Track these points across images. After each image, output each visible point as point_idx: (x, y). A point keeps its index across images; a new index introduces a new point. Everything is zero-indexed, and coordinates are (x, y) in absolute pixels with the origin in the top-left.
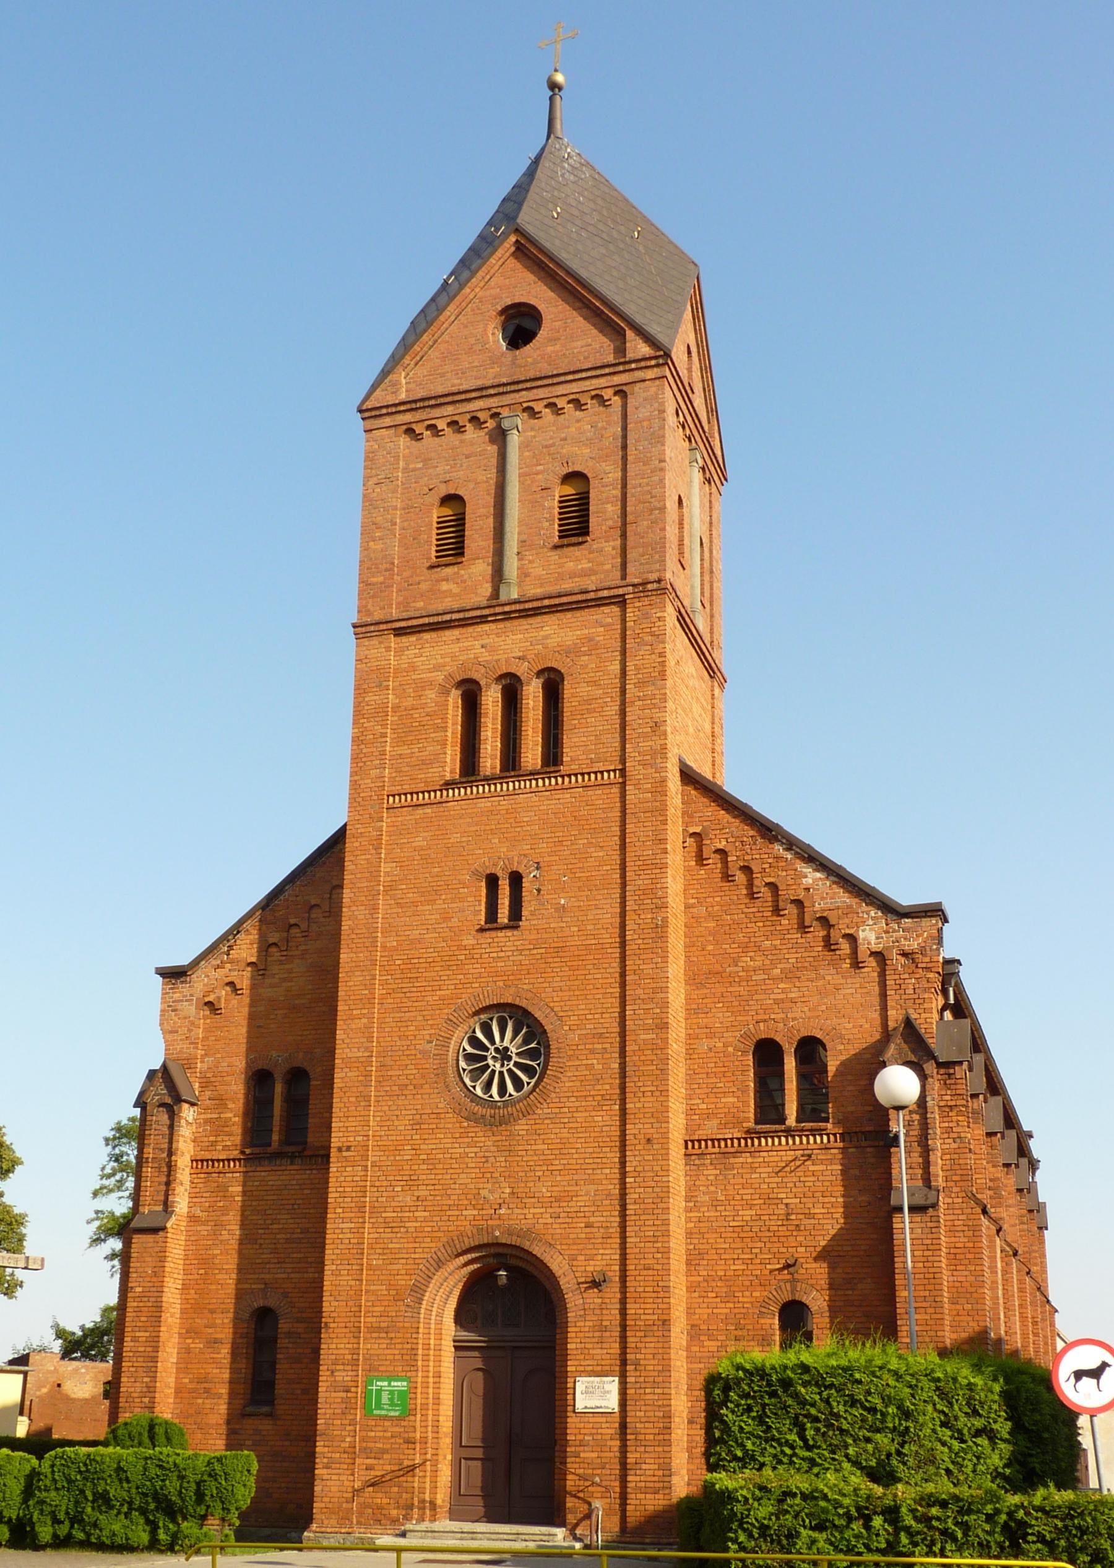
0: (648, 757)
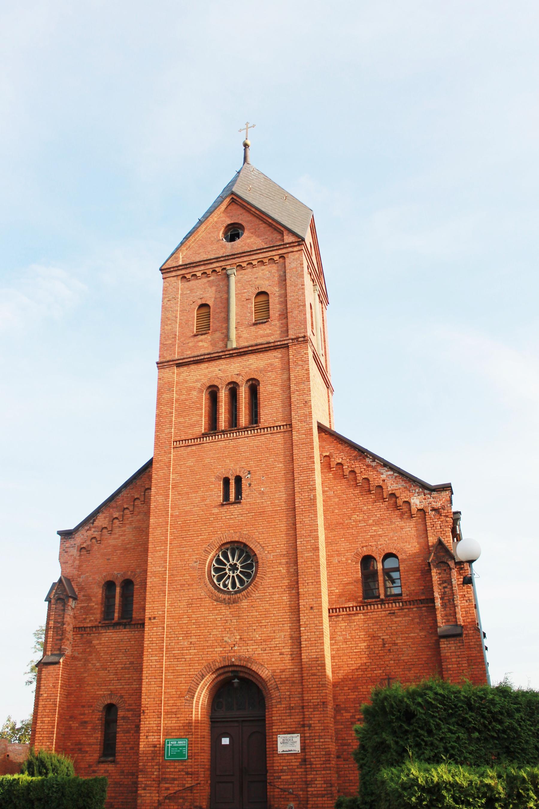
0: (303, 418)
